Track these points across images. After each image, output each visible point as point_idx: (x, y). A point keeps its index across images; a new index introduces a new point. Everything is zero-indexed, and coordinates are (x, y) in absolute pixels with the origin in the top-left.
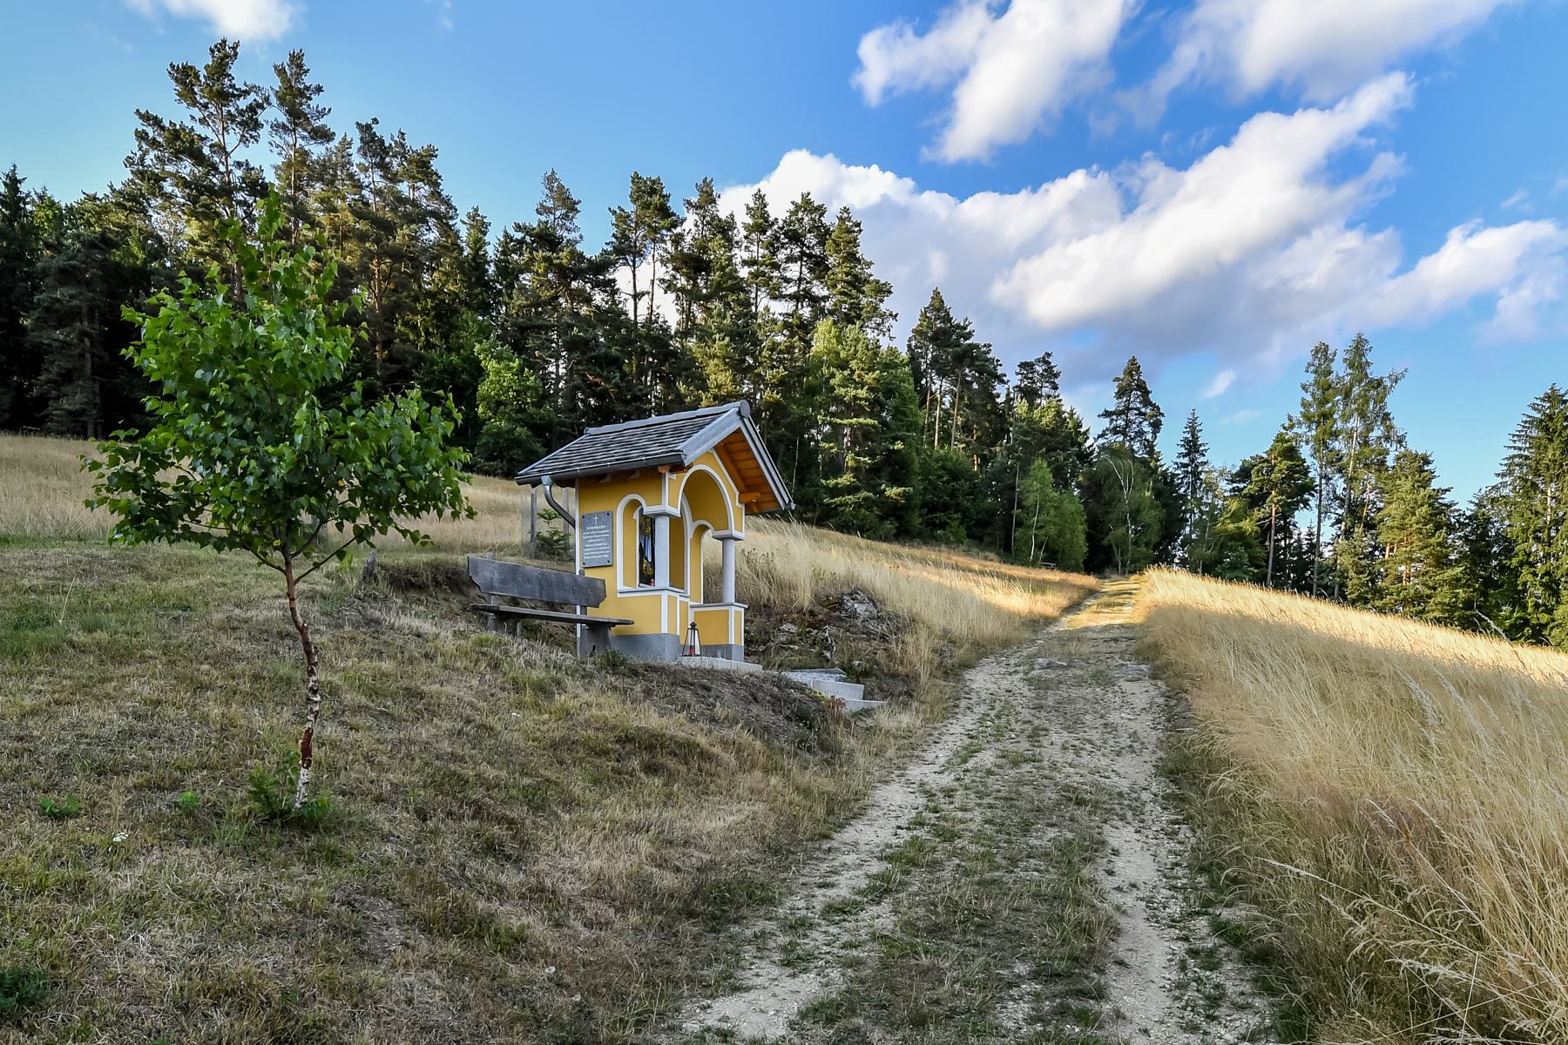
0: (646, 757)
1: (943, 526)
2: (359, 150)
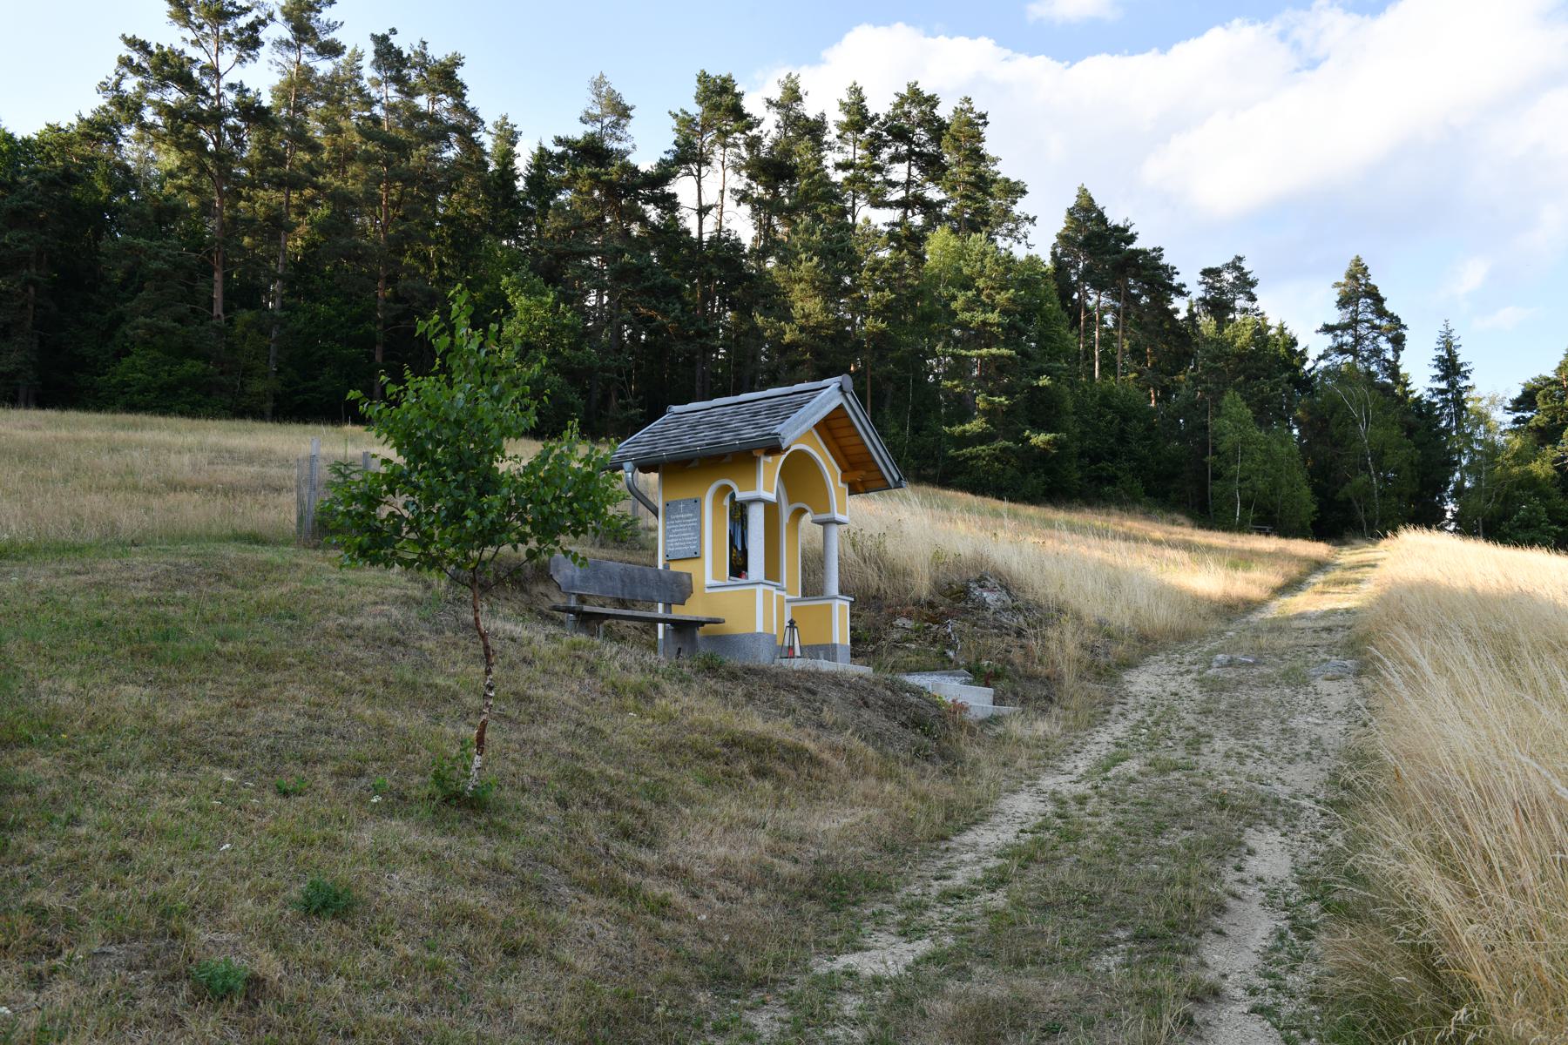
0: (755, 761)
1: (1112, 480)
2: (373, 63)
